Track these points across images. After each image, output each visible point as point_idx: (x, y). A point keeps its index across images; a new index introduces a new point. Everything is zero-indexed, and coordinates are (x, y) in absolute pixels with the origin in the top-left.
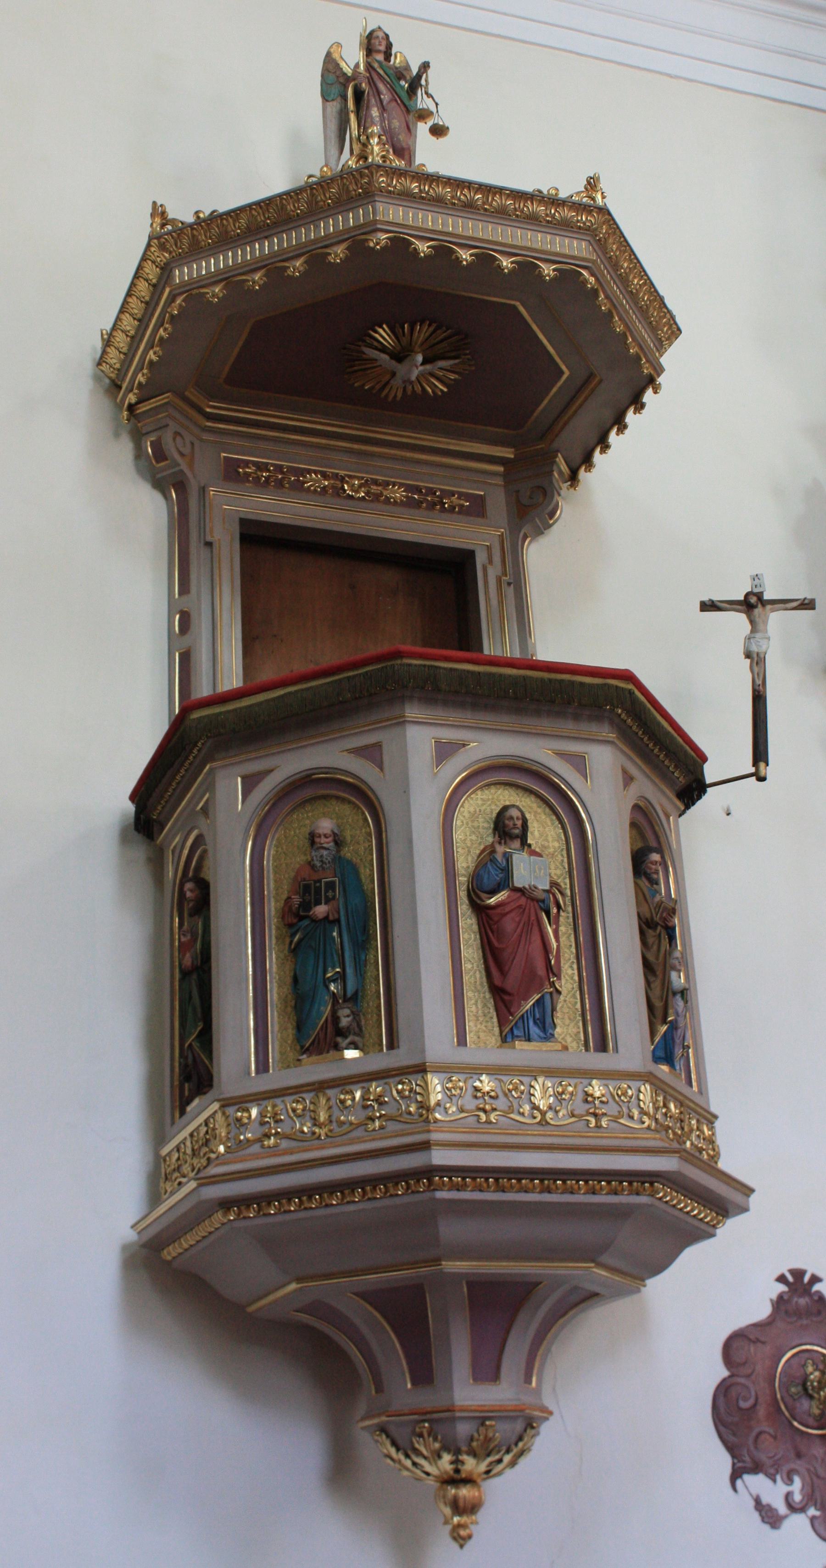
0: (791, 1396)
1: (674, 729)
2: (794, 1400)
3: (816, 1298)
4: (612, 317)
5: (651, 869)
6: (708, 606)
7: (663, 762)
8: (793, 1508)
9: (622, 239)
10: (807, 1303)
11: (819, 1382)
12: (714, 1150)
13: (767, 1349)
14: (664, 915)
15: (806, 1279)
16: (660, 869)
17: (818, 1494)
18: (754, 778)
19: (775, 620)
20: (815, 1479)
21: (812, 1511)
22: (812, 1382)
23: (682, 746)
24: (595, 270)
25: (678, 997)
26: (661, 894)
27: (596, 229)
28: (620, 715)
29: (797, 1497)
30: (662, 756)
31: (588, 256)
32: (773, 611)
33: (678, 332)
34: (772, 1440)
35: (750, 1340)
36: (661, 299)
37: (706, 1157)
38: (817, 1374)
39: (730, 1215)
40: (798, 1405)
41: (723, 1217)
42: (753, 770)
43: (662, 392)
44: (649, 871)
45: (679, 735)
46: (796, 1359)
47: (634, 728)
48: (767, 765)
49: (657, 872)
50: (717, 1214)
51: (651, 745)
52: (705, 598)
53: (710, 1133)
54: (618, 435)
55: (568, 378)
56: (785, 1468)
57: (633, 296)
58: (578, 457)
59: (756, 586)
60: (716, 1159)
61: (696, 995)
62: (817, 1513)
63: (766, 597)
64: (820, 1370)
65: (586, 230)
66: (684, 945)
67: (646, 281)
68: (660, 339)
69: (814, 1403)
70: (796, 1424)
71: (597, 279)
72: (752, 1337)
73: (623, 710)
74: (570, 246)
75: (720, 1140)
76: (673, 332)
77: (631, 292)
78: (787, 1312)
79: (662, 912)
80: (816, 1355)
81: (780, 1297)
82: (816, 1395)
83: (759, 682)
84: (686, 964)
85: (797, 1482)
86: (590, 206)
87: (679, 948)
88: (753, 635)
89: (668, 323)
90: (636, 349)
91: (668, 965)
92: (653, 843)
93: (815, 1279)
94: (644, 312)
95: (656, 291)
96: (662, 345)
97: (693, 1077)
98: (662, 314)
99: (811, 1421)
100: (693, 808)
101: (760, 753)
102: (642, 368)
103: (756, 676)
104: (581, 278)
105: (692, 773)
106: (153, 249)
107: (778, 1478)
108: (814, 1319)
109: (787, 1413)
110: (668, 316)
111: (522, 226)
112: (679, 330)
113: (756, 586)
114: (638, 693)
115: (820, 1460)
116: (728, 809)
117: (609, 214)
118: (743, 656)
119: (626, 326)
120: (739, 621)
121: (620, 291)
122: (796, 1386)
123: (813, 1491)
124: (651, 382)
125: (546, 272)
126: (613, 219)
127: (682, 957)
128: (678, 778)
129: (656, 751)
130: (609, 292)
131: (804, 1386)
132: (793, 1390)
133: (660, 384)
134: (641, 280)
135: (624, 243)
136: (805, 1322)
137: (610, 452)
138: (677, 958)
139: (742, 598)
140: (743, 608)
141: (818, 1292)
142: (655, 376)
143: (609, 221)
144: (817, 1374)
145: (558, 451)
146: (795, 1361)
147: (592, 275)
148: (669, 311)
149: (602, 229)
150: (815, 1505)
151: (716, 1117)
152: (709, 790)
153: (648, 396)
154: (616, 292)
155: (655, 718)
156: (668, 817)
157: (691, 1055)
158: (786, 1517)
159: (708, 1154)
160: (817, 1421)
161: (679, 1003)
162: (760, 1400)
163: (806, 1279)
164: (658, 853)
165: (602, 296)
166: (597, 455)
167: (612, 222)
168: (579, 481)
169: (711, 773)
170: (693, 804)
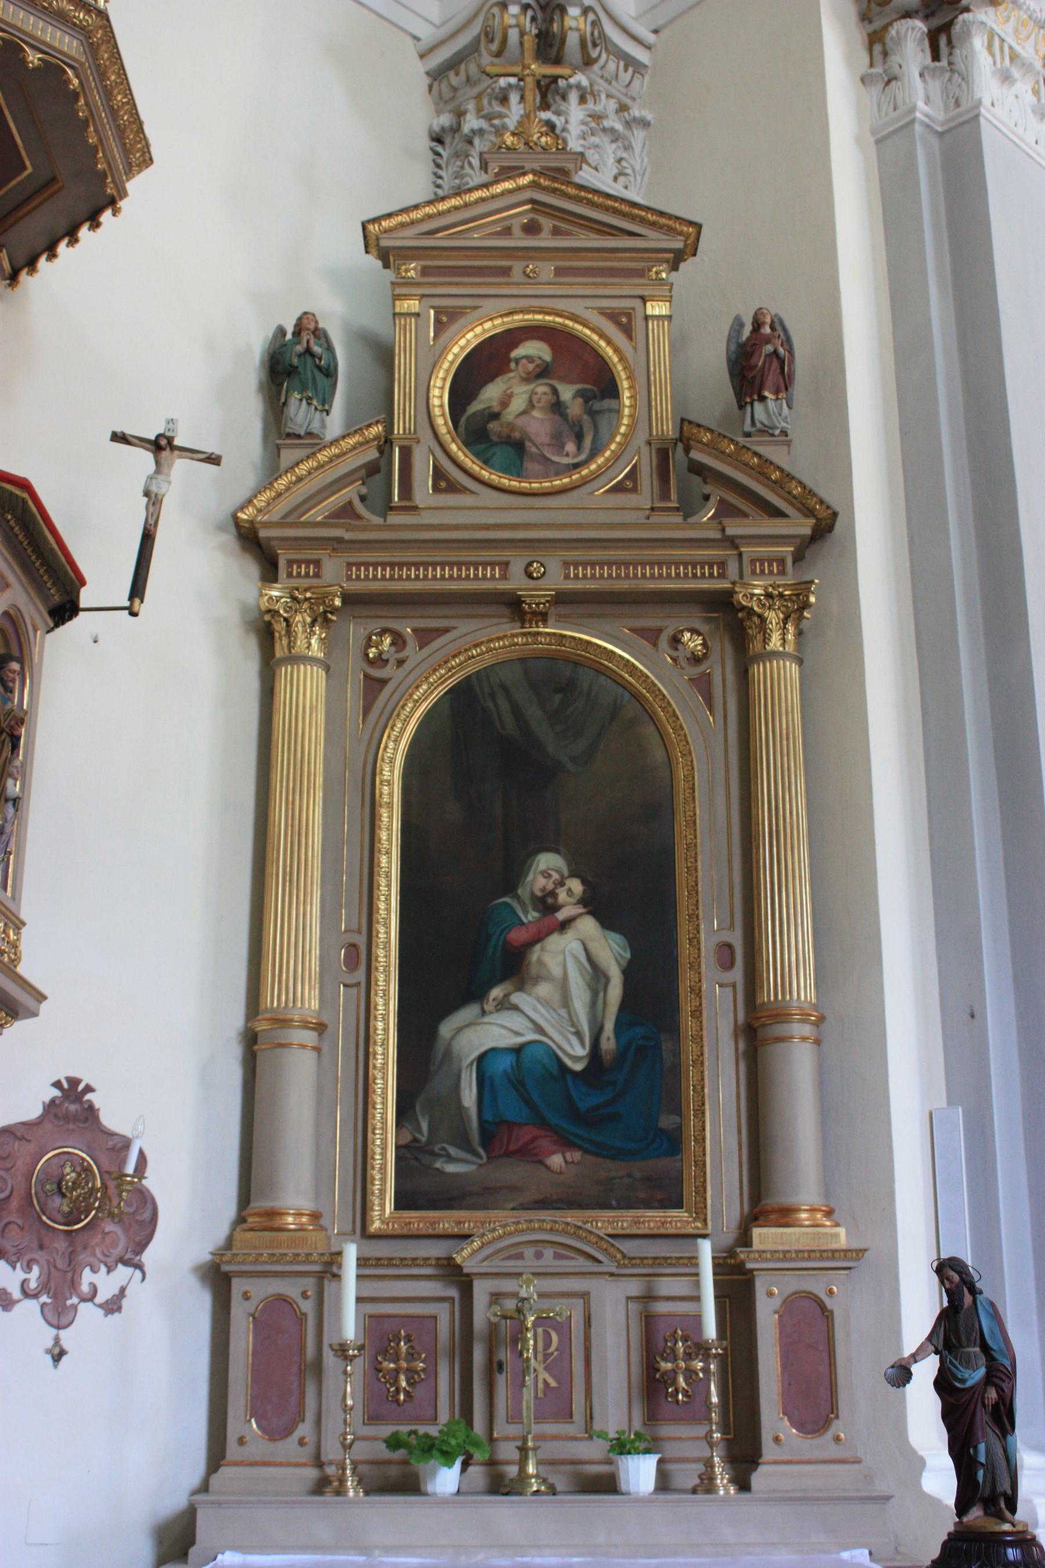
0: (46, 1193)
1: (59, 546)
2: (47, 1196)
3: (86, 1106)
4: (88, 126)
5: (8, 677)
6: (119, 438)
7: (42, 576)
8: (26, 1294)
9: (115, 51)
10: (77, 1110)
11: (74, 1183)
12: (16, 954)
13: (31, 1147)
14: (12, 723)
15: (81, 1087)
16: (17, 678)
17: (52, 1285)
18: (127, 612)
19: (180, 467)
20: (52, 1269)
21: (44, 1299)
22: (67, 1182)
23: (63, 565)
24: (80, 71)
25: (10, 804)
26: (13, 702)
27: (91, 31)
28: (8, 521)
29: (33, 1285)
30: (42, 571)
31: (77, 56)
32: (180, 457)
33: (150, 162)
34: (18, 1230)
35: (16, 1137)
36: (141, 125)
37: (6, 959)
38: (73, 1175)
39: (19, 1017)
40: (50, 1201)
41: (12, 1018)
42: (127, 604)
43: (121, 216)
44: (5, 678)
45: (63, 553)
46: (55, 1161)
47: (21, 537)
48: (142, 602)
49: (13, 681)
50: (7, 1015)
51: (33, 557)
52: (118, 430)
53: (15, 937)
54: (67, 246)
55: (30, 175)
56: (27, 1257)
57: (114, 113)
58: (21, 258)
59: (169, 430)
60: (16, 963)
61: (28, 806)
62: (49, 1301)
63: (177, 442)
64: (77, 1172)
65: (81, 29)
66: (25, 756)
67: (129, 100)
68: (130, 163)
69: (65, 1201)
70: (44, 1218)
71: (81, 83)
72: (19, 1134)
73: (14, 516)
74: (61, 41)
75: (24, 946)
76: (145, 161)
77: (112, 107)
78: (56, 1116)
79: (11, 720)
80: (76, 1157)
81: (53, 1101)
82: (68, 1194)
83: (151, 521)
84: (24, 774)
85: (36, 1270)
86: (90, 5)
87: (21, 757)
88: (155, 476)
89: (141, 150)
90: (105, 166)
91: (5, 772)
92: (16, 653)
93: (89, 1089)
94: (121, 132)
95: (137, 114)
96: (131, 170)
97: (10, 882)
98: (138, 139)
99: (59, 1217)
100: (62, 628)
101: (137, 590)
102: (106, 186)
103: (150, 515)
104: (65, 77)
105: (68, 593)
106: (535, 413)
107: (18, 1265)
108: (81, 1125)
109: (38, 1208)
110: (143, 142)
111: (27, 8)
112: (151, 159)
113: (169, 430)
114: (30, 503)
115: (60, 1253)
116: (96, 637)
117: (108, 20)
118: (142, 494)
119: (100, 139)
120: (145, 459)
121: (102, 102)
122: (52, 1183)
123: (49, 1280)
124: (112, 203)
125: (31, 58)
126: (110, 27)
127: (22, 766)
128: (53, 596)
129: (38, 564)
130: (90, 100)
131: (59, 1184)
132: (48, 1187)
133: (120, 208)
134: (124, 98)
135: (117, 56)
136: (71, 1126)
137: (56, 262)
138: (16, 767)
139: (153, 438)
140: (153, 447)
141: (89, 1101)
142: (118, 198)
143: (106, 27)
144: (73, 1175)
145: (3, 246)
146: (55, 1161)
147: (77, 76)
148: (145, 138)
149: (97, 33)
150: (48, 1293)
151: (24, 924)
152: (81, 614)
153: (106, 217)
154: (97, 102)
155: (43, 533)
156: (35, 630)
157: (11, 861)
158: (19, 1301)
159: (9, 957)
160: (64, 1217)
161: (10, 809)
162: (15, 1193)
163: (81, 1087)
164: (18, 662)
165: (82, 102)
166: (43, 259)
167: (108, 29)
168: (18, 282)
169: (86, 597)
170: (63, 624)
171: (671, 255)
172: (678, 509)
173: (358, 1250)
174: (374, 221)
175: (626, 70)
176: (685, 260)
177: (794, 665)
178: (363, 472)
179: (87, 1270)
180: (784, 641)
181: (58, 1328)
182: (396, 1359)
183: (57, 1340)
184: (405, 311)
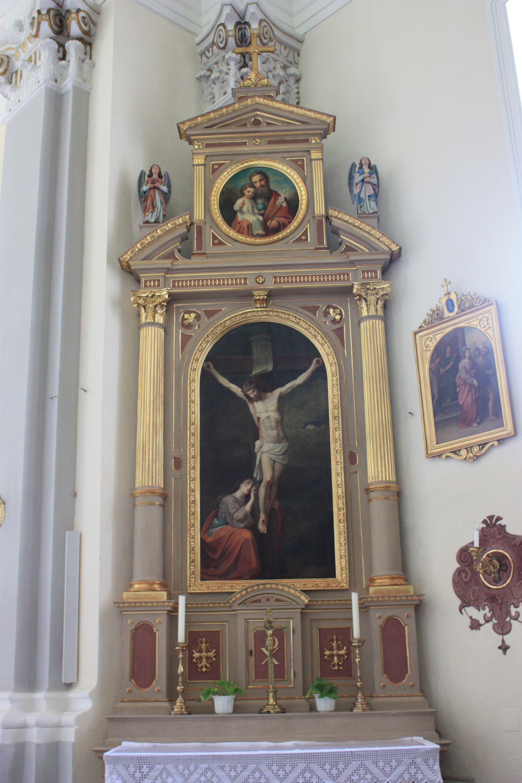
85: (487, 607)
93: (499, 519)
141: (499, 524)
171: (322, 131)
172: (328, 248)
173: (186, 600)
174: (183, 123)
175: (285, 49)
176: (330, 134)
177: (380, 321)
178: (180, 239)
179: (512, 606)
180: (377, 310)
181: (503, 634)
182: (200, 651)
183: (503, 641)
184: (197, 163)
